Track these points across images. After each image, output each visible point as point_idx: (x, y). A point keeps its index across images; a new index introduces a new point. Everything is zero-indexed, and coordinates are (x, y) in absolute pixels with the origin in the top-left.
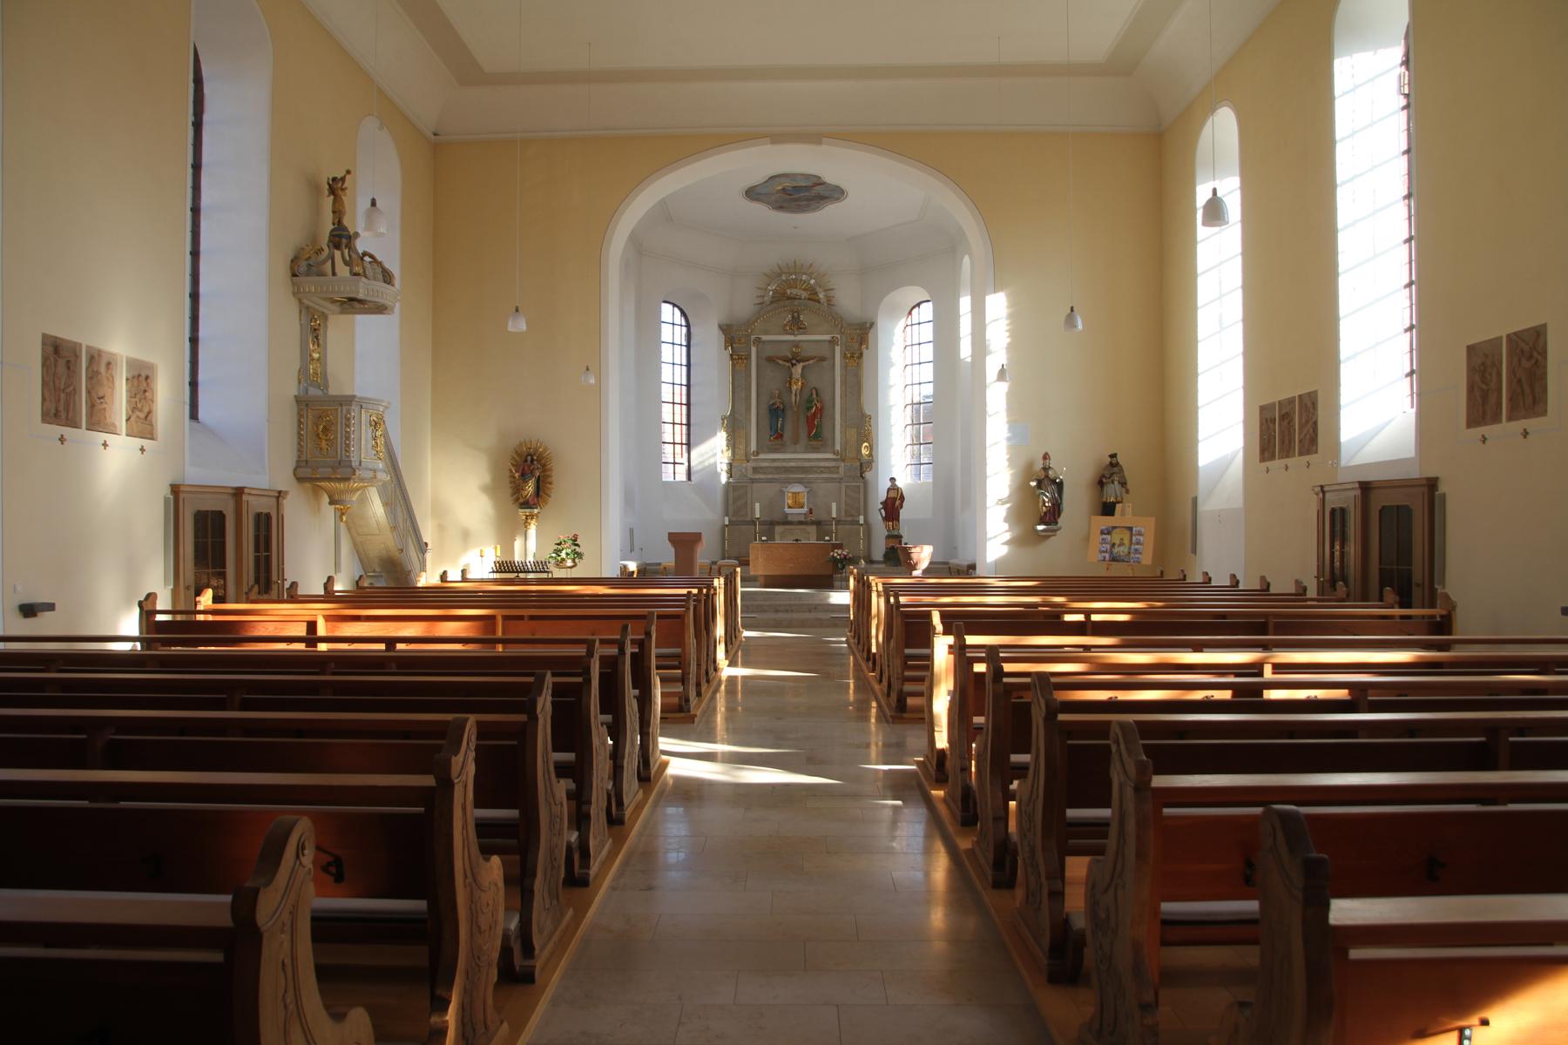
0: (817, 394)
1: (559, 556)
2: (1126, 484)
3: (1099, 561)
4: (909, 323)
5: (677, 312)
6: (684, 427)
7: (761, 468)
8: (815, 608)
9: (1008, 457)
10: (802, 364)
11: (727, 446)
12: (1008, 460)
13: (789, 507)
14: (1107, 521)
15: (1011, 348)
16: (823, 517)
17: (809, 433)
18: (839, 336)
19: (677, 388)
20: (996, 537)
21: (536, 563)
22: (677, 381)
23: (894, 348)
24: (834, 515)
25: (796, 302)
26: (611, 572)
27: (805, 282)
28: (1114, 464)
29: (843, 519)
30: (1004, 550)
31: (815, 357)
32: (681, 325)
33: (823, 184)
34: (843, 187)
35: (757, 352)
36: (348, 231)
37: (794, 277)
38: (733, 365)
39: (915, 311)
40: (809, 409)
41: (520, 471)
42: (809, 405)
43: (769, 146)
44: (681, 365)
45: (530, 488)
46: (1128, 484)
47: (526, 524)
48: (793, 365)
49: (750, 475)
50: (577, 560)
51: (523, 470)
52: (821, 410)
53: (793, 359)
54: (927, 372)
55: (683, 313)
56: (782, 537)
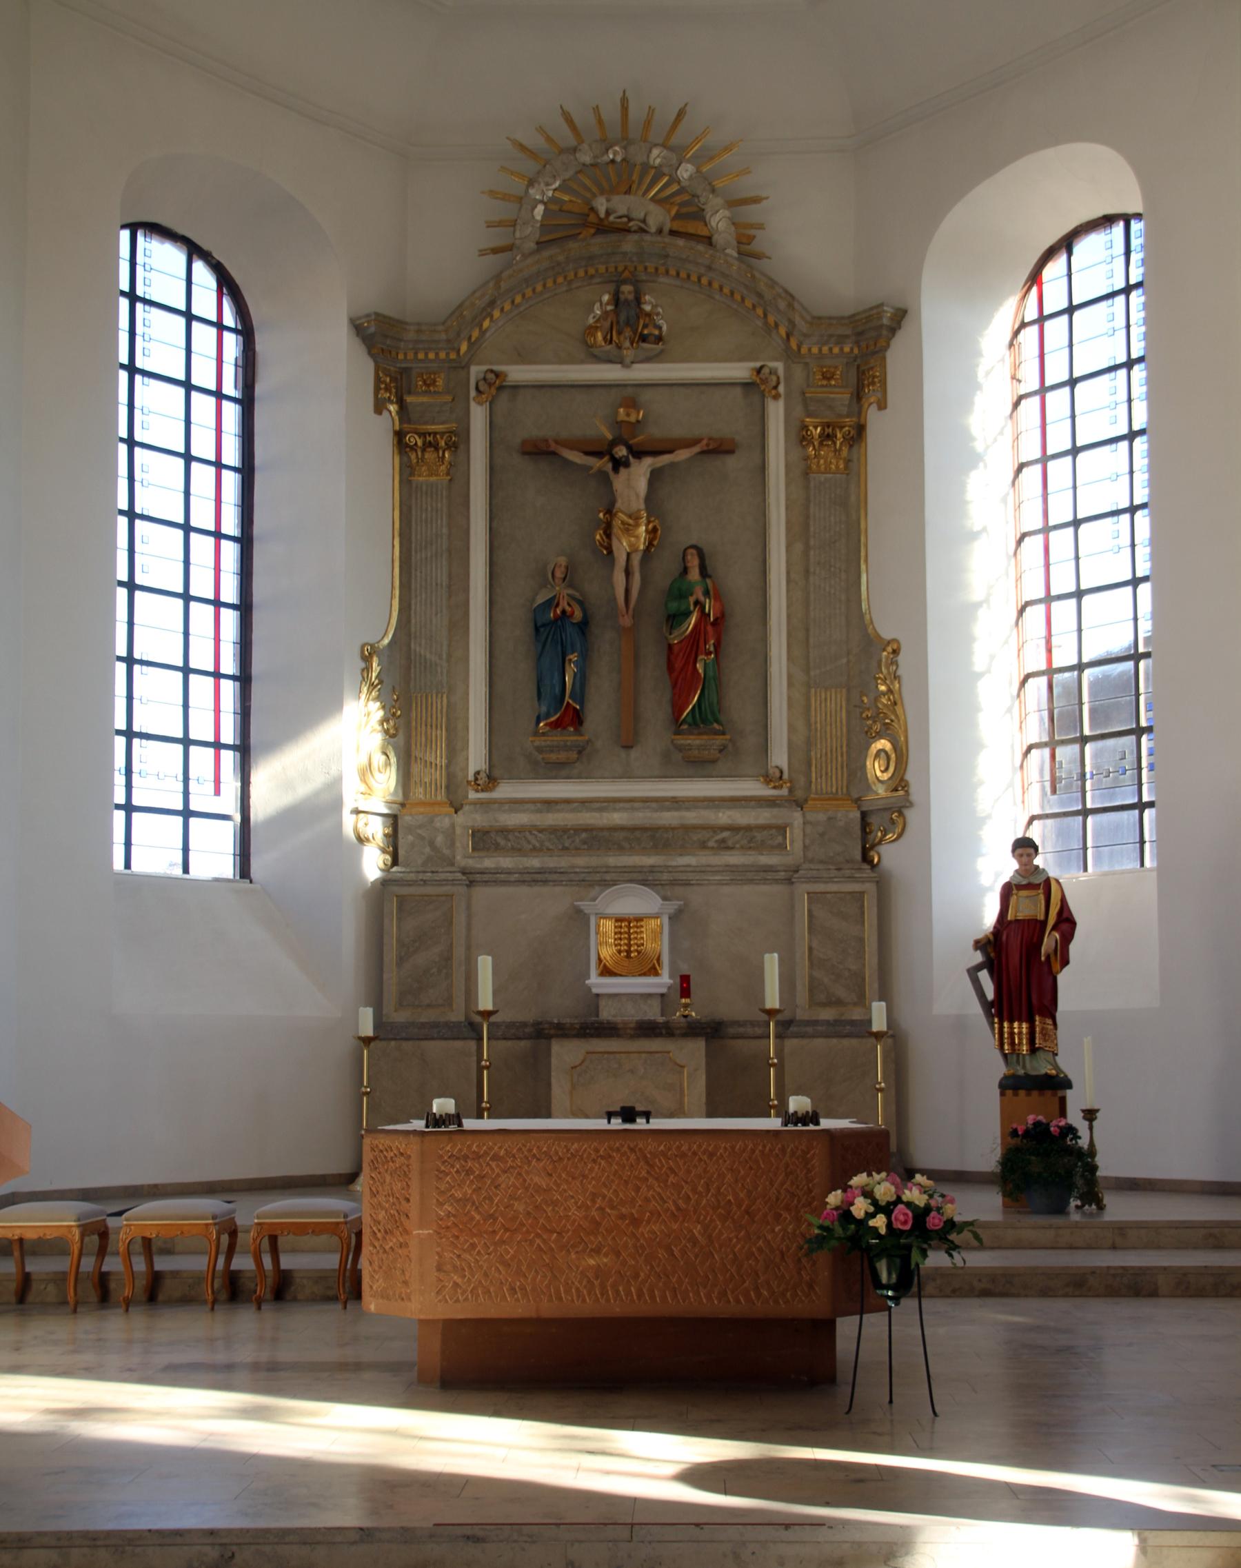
0: (704, 572)
5: (204, 276)
7: (504, 831)
10: (648, 463)
13: (606, 972)
16: (729, 1007)
17: (677, 709)
23: (979, 399)
24: (773, 999)
25: (629, 244)
29: (801, 1015)
35: (491, 425)
38: (407, 473)
39: (1054, 270)
40: (674, 619)
42: (674, 606)
48: (618, 464)
49: (464, 856)
55: (227, 284)
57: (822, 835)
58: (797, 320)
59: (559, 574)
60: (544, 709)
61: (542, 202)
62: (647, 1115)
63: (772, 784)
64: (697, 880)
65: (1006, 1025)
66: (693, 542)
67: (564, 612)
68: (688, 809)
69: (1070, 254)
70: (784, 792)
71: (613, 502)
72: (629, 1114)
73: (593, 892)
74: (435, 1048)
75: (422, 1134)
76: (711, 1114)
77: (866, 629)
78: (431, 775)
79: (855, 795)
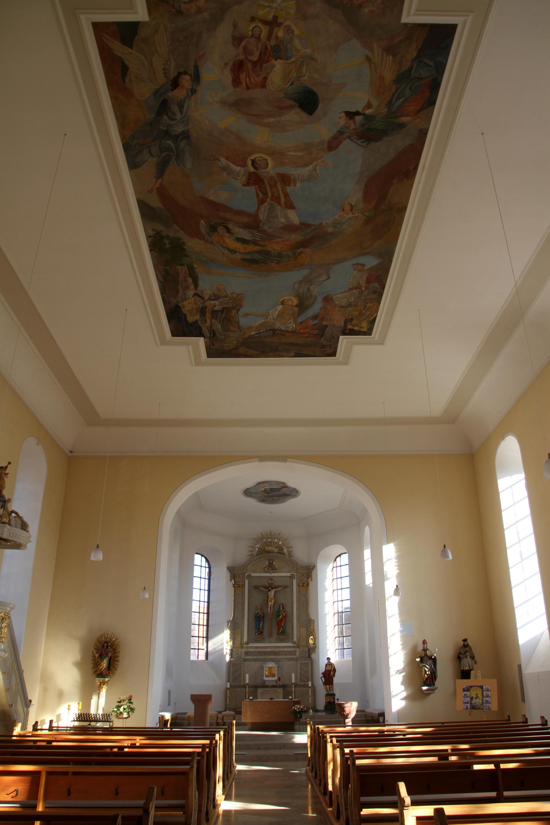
1: (119, 710)
2: (474, 658)
3: (463, 709)
4: (335, 566)
6: (205, 639)
7: (250, 652)
8: (284, 746)
9: (401, 643)
10: (274, 590)
11: (230, 638)
12: (402, 644)
13: (267, 676)
14: (465, 683)
15: (399, 576)
17: (279, 631)
18: (295, 574)
19: (202, 603)
20: (397, 695)
21: (103, 715)
22: (202, 599)
24: (293, 681)
25: (271, 554)
26: (151, 722)
27: (276, 543)
28: (465, 645)
29: (299, 683)
30: (403, 704)
31: (282, 586)
32: (206, 567)
33: (287, 487)
34: (297, 489)
35: (249, 583)
36: (5, 498)
37: (270, 540)
38: (235, 591)
39: (338, 559)
40: (279, 616)
41: (100, 652)
43: (258, 462)
44: (205, 590)
45: (104, 664)
46: (475, 658)
47: (100, 688)
48: (269, 590)
49: (243, 656)
50: (130, 713)
51: (101, 652)
52: (285, 617)
53: (269, 587)
54: (346, 594)
55: (207, 560)
56: (263, 698)
58: (298, 566)
59: (259, 608)
60: (257, 631)
61: (257, 548)
62: (274, 699)
65: (54, 728)
66: (281, 603)
67: (260, 615)
68: (280, 648)
69: (340, 557)
70: (296, 645)
71: (268, 596)
72: (271, 699)
73: (264, 663)
74: (238, 689)
75: (249, 701)
76: (283, 699)
77: (309, 618)
78: (238, 642)
79: (307, 645)
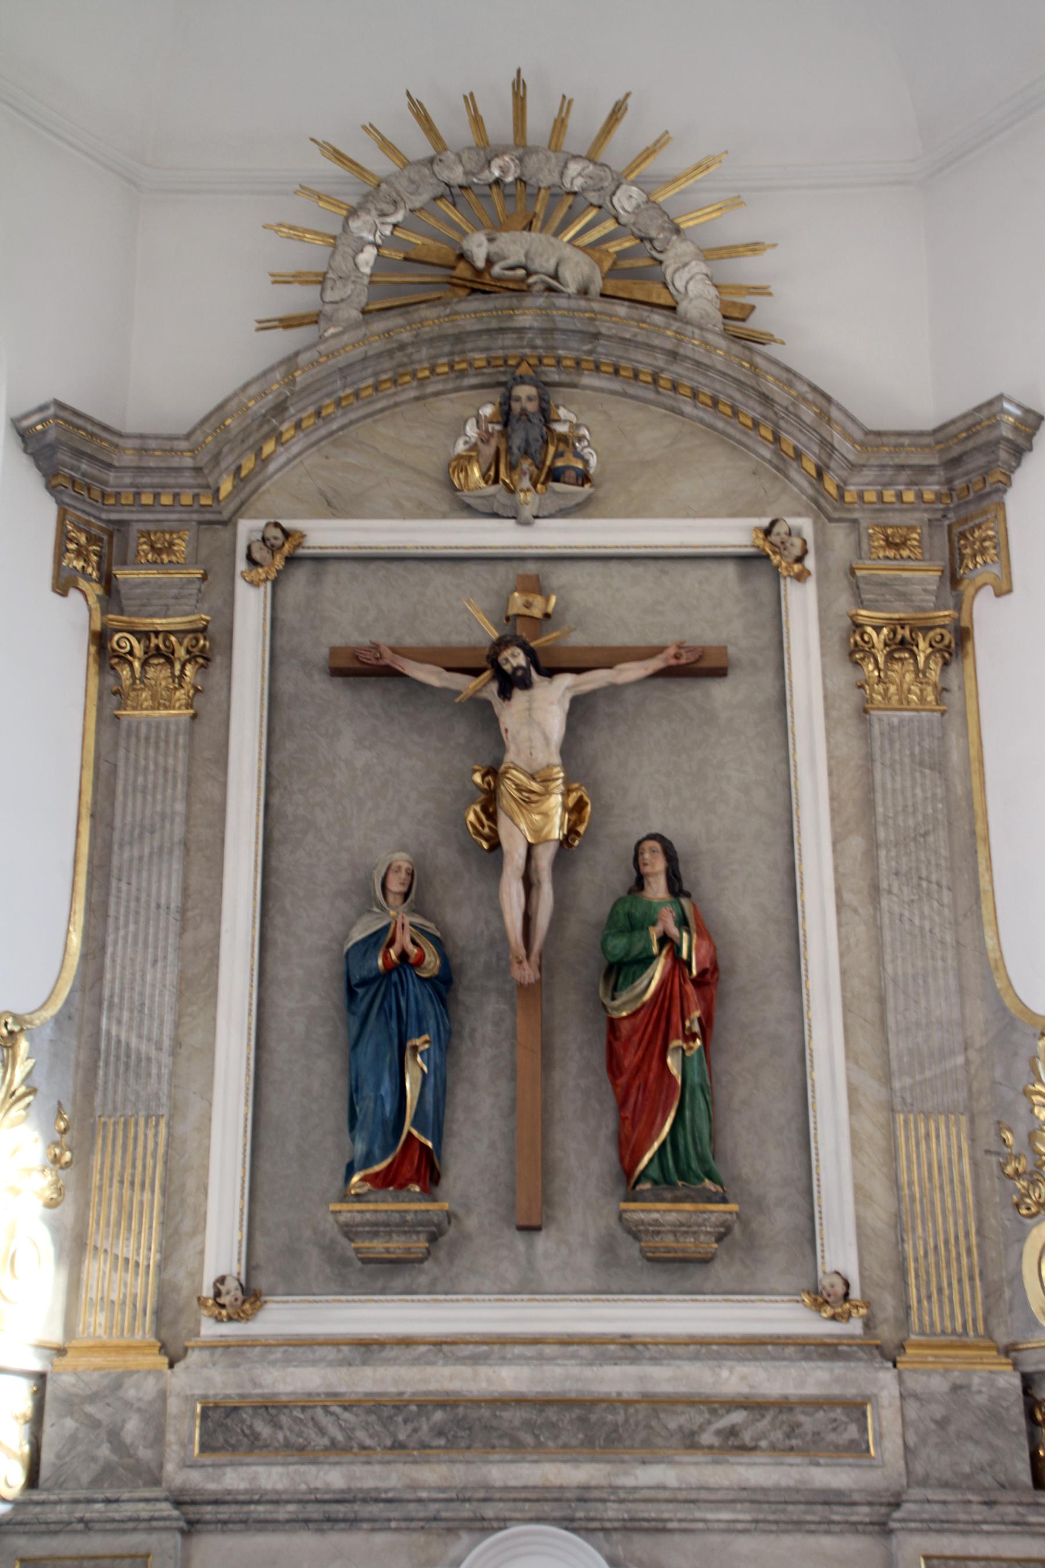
10: (565, 681)
57: (942, 1424)
59: (396, 885)
60: (360, 1148)
63: (829, 1311)
64: (680, 1520)
66: (656, 829)
67: (403, 955)
68: (655, 1360)
70: (855, 1327)
